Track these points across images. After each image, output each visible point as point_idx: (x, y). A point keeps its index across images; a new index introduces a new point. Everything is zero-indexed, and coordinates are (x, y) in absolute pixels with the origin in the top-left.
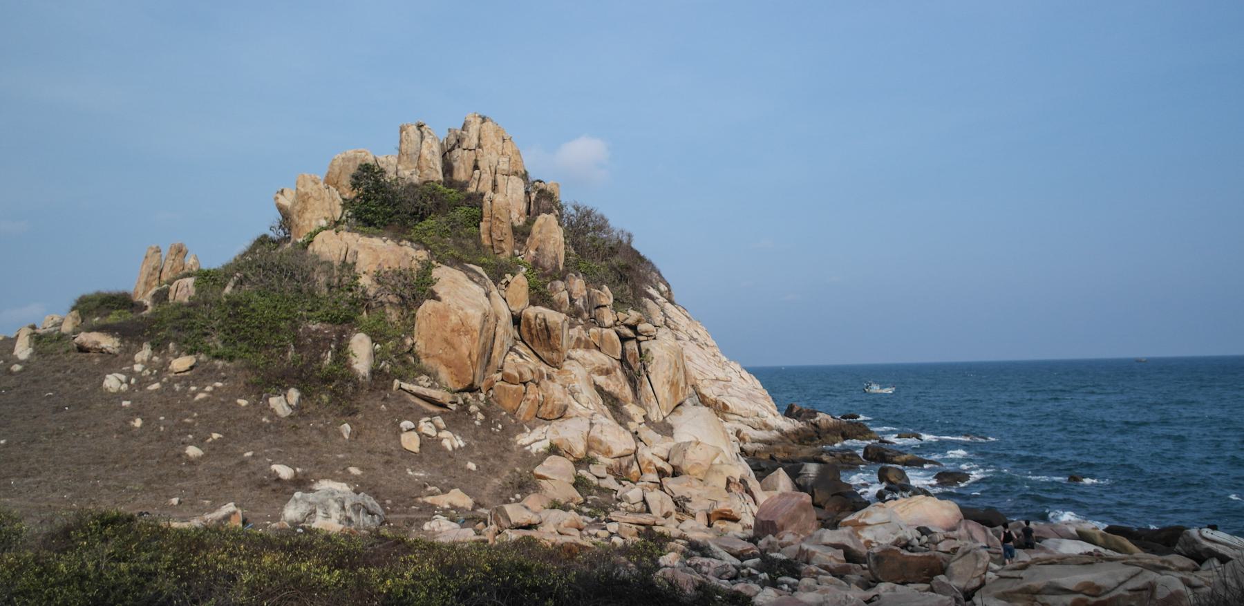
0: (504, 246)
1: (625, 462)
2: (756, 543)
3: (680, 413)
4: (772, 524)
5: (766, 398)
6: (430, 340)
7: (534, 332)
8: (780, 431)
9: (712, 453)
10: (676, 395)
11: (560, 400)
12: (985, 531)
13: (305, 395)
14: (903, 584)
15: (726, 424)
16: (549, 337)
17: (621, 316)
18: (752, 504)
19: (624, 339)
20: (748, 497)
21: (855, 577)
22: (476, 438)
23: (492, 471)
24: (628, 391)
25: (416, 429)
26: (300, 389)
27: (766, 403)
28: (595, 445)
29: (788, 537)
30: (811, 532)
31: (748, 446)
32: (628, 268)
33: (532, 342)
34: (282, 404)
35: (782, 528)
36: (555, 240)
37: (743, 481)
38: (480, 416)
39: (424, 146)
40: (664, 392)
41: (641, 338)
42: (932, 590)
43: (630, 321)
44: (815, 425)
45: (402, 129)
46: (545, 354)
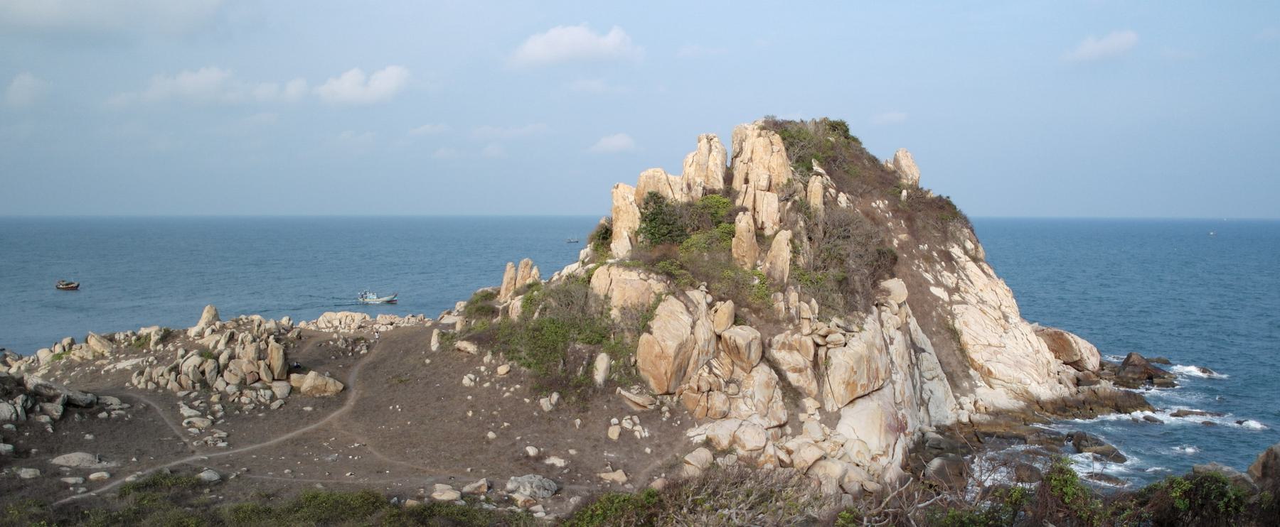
1: (754, 455)
6: (644, 361)
13: (562, 397)
19: (817, 345)
22: (659, 430)
23: (659, 455)
25: (620, 423)
26: (560, 393)
32: (845, 279)
34: (546, 403)
38: (667, 415)
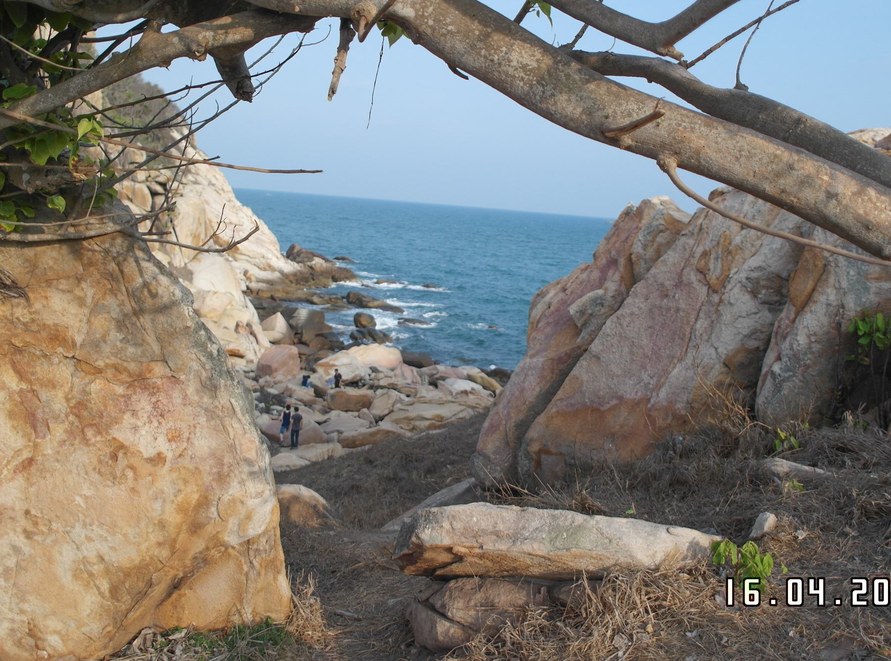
2: (257, 381)
3: (200, 261)
4: (269, 367)
5: (271, 243)
8: (281, 272)
12: (412, 371)
14: (346, 411)
15: (234, 263)
17: (154, 173)
18: (255, 344)
19: (154, 194)
20: (252, 338)
21: (318, 407)
27: (271, 247)
29: (279, 376)
30: (295, 372)
31: (254, 285)
35: (276, 370)
37: (249, 325)
42: (359, 417)
43: (162, 179)
44: (311, 267)
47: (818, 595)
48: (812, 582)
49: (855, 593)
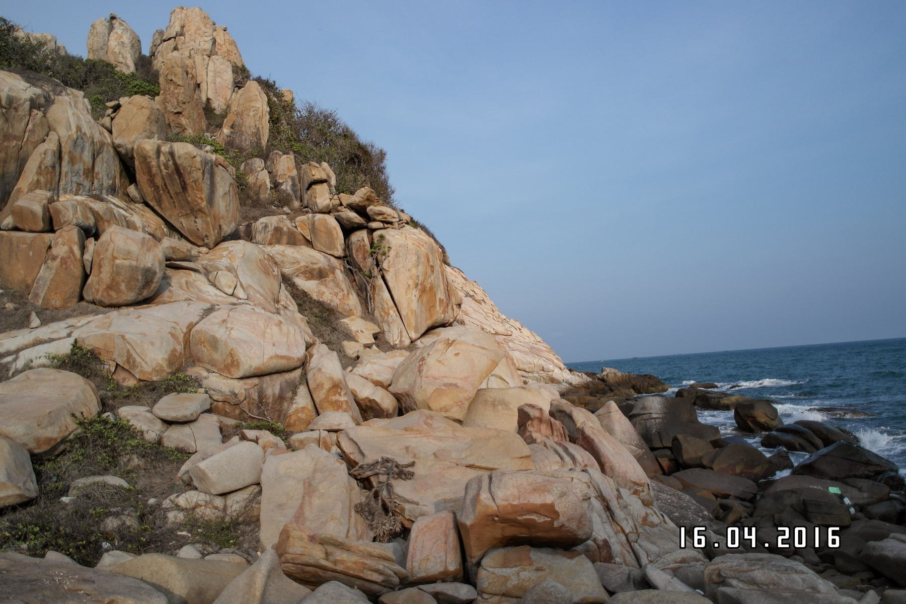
0: (184, 121)
7: (158, 181)
9: (481, 361)
10: (431, 307)
11: (128, 254)
16: (184, 188)
19: (348, 230)
24: (353, 301)
27: (551, 356)
28: (205, 351)
33: (159, 202)
36: (257, 109)
39: (113, 36)
40: (409, 299)
41: (374, 225)
44: (603, 380)
45: (93, 26)
46: (184, 223)
47: (751, 540)
48: (746, 529)
49: (780, 538)
